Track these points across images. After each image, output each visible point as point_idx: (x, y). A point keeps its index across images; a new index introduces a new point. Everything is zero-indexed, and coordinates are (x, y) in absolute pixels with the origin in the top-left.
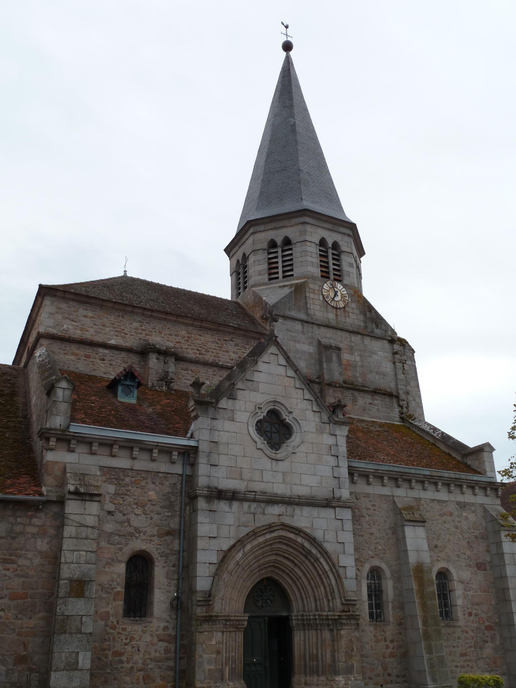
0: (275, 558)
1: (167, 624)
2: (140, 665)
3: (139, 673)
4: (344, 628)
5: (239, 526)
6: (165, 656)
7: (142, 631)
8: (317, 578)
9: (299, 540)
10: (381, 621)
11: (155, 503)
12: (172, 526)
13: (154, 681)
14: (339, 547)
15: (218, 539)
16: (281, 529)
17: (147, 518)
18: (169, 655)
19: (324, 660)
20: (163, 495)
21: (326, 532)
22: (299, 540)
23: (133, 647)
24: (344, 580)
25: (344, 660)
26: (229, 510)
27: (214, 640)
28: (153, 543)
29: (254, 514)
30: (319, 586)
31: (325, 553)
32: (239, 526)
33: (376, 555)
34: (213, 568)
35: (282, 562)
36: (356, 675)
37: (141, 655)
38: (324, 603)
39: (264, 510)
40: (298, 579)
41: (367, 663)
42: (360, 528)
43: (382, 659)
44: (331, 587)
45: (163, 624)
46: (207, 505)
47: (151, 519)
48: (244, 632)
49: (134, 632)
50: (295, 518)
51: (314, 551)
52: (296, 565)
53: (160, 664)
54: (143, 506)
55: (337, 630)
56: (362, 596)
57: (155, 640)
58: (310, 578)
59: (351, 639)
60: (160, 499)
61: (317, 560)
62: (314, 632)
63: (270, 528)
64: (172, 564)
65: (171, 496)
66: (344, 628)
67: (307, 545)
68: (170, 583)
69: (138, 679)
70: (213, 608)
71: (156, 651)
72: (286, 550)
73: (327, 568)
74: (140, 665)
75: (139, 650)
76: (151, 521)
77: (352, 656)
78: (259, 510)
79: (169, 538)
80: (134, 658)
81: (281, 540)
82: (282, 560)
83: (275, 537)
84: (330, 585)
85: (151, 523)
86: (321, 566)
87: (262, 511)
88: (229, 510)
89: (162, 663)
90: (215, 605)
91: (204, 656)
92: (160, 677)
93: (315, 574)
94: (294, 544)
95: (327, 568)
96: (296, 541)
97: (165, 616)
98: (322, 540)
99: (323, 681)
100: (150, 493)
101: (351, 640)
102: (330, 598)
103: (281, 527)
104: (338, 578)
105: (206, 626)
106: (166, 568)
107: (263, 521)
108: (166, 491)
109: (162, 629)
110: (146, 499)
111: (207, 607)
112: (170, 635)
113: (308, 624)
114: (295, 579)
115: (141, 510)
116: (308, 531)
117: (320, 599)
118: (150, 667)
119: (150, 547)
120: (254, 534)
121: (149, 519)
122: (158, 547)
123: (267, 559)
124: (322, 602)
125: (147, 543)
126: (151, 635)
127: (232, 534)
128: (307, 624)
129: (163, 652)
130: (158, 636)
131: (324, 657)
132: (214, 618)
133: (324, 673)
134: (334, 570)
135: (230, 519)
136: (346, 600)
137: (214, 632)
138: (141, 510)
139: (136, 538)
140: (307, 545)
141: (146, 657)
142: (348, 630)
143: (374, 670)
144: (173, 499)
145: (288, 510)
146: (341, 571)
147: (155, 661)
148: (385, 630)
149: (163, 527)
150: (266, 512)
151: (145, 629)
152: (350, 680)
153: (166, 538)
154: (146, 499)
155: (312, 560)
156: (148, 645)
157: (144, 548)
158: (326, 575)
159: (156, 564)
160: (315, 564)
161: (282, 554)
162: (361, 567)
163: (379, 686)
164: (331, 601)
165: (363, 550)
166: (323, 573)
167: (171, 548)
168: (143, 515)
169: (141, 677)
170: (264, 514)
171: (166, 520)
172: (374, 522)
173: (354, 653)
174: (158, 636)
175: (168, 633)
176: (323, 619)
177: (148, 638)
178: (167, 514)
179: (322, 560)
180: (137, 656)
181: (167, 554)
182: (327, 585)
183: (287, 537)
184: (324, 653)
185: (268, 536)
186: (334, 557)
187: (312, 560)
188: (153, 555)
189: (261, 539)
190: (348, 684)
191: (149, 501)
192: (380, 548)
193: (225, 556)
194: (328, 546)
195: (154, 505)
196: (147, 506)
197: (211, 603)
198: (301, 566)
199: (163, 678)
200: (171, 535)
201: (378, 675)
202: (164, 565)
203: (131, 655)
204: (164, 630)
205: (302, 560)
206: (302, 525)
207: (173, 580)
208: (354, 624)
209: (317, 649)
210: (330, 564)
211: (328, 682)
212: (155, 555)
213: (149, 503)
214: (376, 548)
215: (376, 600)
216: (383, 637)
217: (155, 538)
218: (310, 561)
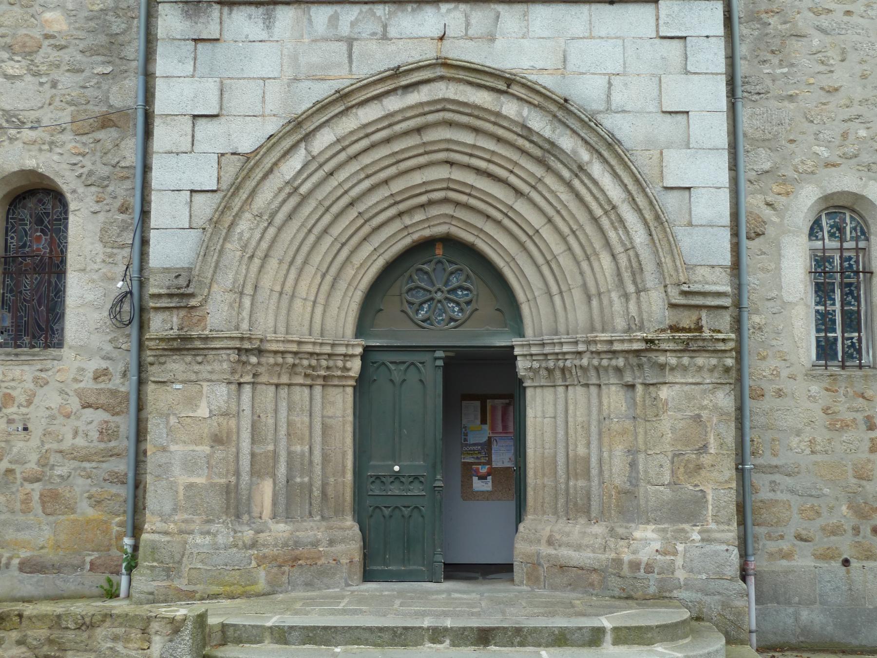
0: (446, 176)
1: (104, 364)
2: (32, 466)
3: (28, 487)
4: (670, 378)
5: (296, 79)
6: (102, 446)
7: (36, 380)
8: (590, 229)
9: (510, 108)
10: (860, 367)
11: (63, 43)
12: (117, 101)
13: (73, 510)
14: (668, 127)
15: (223, 120)
16: (441, 78)
17: (41, 84)
18: (113, 444)
19: (606, 474)
20: (89, 19)
21: (616, 81)
22: (510, 108)
23: (10, 421)
24: (681, 233)
25: (667, 478)
26: (264, 35)
27: (204, 404)
28: (59, 150)
29: (350, 42)
30: (597, 254)
31: (610, 148)
32: (296, 79)
33: (845, 156)
34: (205, 206)
35: (472, 187)
36: (713, 526)
37: (35, 442)
38: (611, 303)
39: (385, 27)
40: (530, 237)
41: (792, 492)
42: (785, 75)
43: (854, 481)
44: (631, 253)
45: (96, 364)
46: (188, 23)
47: (54, 85)
48: (363, 386)
49: (12, 384)
50: (499, 44)
51: (567, 142)
52: (518, 193)
53: (86, 465)
54: (30, 53)
55: (646, 385)
56: (780, 288)
57: (74, 403)
58: (566, 230)
59: (699, 416)
60: (78, 29)
61: (581, 169)
62: (580, 390)
63: (398, 79)
64: (118, 204)
65: (113, 19)
66: (670, 378)
67: (538, 123)
68: (111, 256)
69: (27, 500)
70: (202, 319)
71: (76, 433)
72: (474, 146)
73: (615, 193)
74: (32, 466)
75: (25, 429)
76: (54, 91)
77: (699, 467)
78: (369, 27)
79: (107, 136)
80: (15, 450)
81: (449, 116)
82: (470, 178)
83: (422, 104)
84: (630, 248)
85: (52, 97)
86: (595, 191)
87: (380, 30)
88: (264, 35)
89: (94, 464)
90: (210, 307)
91: (173, 448)
92: (89, 498)
93: (582, 216)
94: (495, 124)
95: (615, 193)
96: (498, 114)
97: (101, 341)
98: (597, 105)
99: (596, 536)
100: (48, 15)
101: (697, 418)
102: (631, 288)
103: (440, 71)
104: (657, 222)
105: (176, 366)
106: (101, 217)
107: (374, 59)
108: (96, 8)
109: (91, 375)
110: (37, 34)
111: (182, 313)
112: (114, 393)
113: (563, 370)
114: (523, 238)
115: (24, 63)
116: (546, 81)
117: (599, 294)
118: (58, 471)
119: (56, 164)
120: (344, 100)
121: (47, 86)
122: (75, 160)
123: (417, 178)
124: (605, 302)
125: (40, 150)
126: (62, 392)
127: (272, 105)
128: (561, 372)
129: (95, 435)
130: (79, 394)
131: (605, 467)
132: (198, 344)
133: (603, 515)
134: (641, 200)
135: (265, 61)
136: (685, 294)
137: (205, 384)
138: (24, 63)
139: (10, 139)
140: (538, 123)
141: (47, 447)
142: (686, 388)
143: (818, 513)
144: (117, 26)
145: (473, 21)
146: (671, 203)
147: (74, 459)
148: (869, 393)
149: (89, 107)
150: (392, 32)
151: (43, 375)
152: (686, 540)
153: (101, 135)
154: (37, 34)
155: (566, 174)
156: (53, 417)
157: (30, 163)
158: (613, 217)
159: (72, 206)
160: (576, 183)
161: (465, 159)
162: (783, 199)
163: (837, 565)
164: (633, 297)
165: (792, 141)
166: (606, 212)
167: (114, 162)
168: (29, 78)
169: (36, 496)
170: (385, 37)
171: (98, 86)
172: (843, 51)
173: (706, 460)
174: (79, 394)
175: (110, 386)
176: (598, 353)
177: (54, 400)
178: (99, 69)
179: (597, 169)
180: (21, 444)
181: (103, 179)
182: (618, 249)
183: (465, 104)
184: (606, 455)
185: (393, 104)
186: (644, 162)
187: (566, 174)
188: (59, 181)
189: (370, 113)
190: (675, 553)
191: (47, 37)
192: (862, 133)
193: (250, 168)
194: (621, 126)
195: (62, 48)
196: (42, 52)
197: (193, 302)
198: (534, 195)
199: (99, 502)
200: (115, 126)
201: (835, 531)
202: (96, 208)
203: (7, 441)
204: (96, 379)
205: (532, 175)
206: (526, 64)
207: (122, 247)
208: (712, 370)
209: (588, 444)
210: (627, 180)
211: (612, 543)
212: (67, 182)
213: (46, 42)
214: (845, 135)
215: (843, 303)
216: (860, 417)
217: (68, 137)
218: (560, 178)
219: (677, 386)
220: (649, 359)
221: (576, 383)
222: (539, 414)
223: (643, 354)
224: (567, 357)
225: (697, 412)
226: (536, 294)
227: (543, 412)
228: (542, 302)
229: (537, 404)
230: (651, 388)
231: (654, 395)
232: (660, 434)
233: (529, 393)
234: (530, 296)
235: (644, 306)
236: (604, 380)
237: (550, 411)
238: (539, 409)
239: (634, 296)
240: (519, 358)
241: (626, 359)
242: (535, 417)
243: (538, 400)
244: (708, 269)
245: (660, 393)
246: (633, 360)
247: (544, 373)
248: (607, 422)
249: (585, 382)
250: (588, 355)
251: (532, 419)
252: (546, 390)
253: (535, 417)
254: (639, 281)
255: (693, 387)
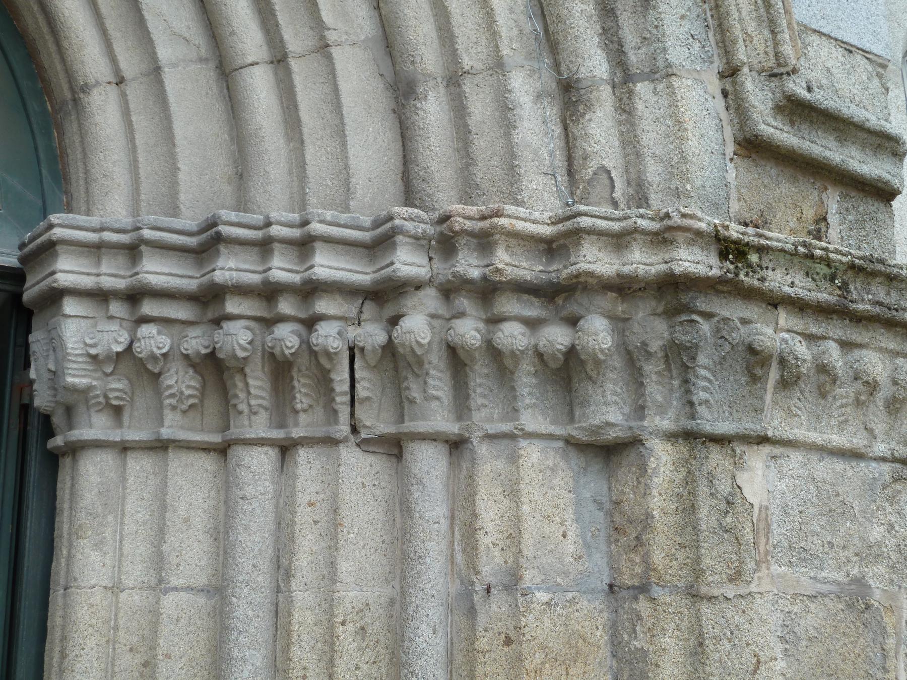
38: (505, 111)
62: (358, 468)
101: (856, 598)
102: (594, 64)
176: (487, 291)
219: (796, 458)
220: (722, 325)
221: (343, 429)
222: (136, 572)
223: (702, 304)
224: (323, 306)
225: (855, 572)
226: (164, 53)
227: (159, 562)
228: (188, 89)
229: (130, 526)
230: (716, 458)
231: (724, 488)
232: (748, 659)
233: (91, 477)
234: (130, 64)
235: (651, 136)
236: (486, 415)
237: (191, 557)
238: (137, 549)
239: (605, 95)
240: (70, 306)
241: (619, 323)
242: (116, 588)
243: (137, 510)
244: (839, 53)
245: (742, 478)
246: (652, 330)
247: (181, 381)
248: (498, 605)
249: (385, 427)
250: (429, 299)
251: (98, 597)
252: (177, 462)
253: (116, 588)
254: (630, 38)
255: (839, 465)
